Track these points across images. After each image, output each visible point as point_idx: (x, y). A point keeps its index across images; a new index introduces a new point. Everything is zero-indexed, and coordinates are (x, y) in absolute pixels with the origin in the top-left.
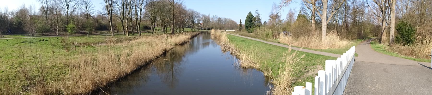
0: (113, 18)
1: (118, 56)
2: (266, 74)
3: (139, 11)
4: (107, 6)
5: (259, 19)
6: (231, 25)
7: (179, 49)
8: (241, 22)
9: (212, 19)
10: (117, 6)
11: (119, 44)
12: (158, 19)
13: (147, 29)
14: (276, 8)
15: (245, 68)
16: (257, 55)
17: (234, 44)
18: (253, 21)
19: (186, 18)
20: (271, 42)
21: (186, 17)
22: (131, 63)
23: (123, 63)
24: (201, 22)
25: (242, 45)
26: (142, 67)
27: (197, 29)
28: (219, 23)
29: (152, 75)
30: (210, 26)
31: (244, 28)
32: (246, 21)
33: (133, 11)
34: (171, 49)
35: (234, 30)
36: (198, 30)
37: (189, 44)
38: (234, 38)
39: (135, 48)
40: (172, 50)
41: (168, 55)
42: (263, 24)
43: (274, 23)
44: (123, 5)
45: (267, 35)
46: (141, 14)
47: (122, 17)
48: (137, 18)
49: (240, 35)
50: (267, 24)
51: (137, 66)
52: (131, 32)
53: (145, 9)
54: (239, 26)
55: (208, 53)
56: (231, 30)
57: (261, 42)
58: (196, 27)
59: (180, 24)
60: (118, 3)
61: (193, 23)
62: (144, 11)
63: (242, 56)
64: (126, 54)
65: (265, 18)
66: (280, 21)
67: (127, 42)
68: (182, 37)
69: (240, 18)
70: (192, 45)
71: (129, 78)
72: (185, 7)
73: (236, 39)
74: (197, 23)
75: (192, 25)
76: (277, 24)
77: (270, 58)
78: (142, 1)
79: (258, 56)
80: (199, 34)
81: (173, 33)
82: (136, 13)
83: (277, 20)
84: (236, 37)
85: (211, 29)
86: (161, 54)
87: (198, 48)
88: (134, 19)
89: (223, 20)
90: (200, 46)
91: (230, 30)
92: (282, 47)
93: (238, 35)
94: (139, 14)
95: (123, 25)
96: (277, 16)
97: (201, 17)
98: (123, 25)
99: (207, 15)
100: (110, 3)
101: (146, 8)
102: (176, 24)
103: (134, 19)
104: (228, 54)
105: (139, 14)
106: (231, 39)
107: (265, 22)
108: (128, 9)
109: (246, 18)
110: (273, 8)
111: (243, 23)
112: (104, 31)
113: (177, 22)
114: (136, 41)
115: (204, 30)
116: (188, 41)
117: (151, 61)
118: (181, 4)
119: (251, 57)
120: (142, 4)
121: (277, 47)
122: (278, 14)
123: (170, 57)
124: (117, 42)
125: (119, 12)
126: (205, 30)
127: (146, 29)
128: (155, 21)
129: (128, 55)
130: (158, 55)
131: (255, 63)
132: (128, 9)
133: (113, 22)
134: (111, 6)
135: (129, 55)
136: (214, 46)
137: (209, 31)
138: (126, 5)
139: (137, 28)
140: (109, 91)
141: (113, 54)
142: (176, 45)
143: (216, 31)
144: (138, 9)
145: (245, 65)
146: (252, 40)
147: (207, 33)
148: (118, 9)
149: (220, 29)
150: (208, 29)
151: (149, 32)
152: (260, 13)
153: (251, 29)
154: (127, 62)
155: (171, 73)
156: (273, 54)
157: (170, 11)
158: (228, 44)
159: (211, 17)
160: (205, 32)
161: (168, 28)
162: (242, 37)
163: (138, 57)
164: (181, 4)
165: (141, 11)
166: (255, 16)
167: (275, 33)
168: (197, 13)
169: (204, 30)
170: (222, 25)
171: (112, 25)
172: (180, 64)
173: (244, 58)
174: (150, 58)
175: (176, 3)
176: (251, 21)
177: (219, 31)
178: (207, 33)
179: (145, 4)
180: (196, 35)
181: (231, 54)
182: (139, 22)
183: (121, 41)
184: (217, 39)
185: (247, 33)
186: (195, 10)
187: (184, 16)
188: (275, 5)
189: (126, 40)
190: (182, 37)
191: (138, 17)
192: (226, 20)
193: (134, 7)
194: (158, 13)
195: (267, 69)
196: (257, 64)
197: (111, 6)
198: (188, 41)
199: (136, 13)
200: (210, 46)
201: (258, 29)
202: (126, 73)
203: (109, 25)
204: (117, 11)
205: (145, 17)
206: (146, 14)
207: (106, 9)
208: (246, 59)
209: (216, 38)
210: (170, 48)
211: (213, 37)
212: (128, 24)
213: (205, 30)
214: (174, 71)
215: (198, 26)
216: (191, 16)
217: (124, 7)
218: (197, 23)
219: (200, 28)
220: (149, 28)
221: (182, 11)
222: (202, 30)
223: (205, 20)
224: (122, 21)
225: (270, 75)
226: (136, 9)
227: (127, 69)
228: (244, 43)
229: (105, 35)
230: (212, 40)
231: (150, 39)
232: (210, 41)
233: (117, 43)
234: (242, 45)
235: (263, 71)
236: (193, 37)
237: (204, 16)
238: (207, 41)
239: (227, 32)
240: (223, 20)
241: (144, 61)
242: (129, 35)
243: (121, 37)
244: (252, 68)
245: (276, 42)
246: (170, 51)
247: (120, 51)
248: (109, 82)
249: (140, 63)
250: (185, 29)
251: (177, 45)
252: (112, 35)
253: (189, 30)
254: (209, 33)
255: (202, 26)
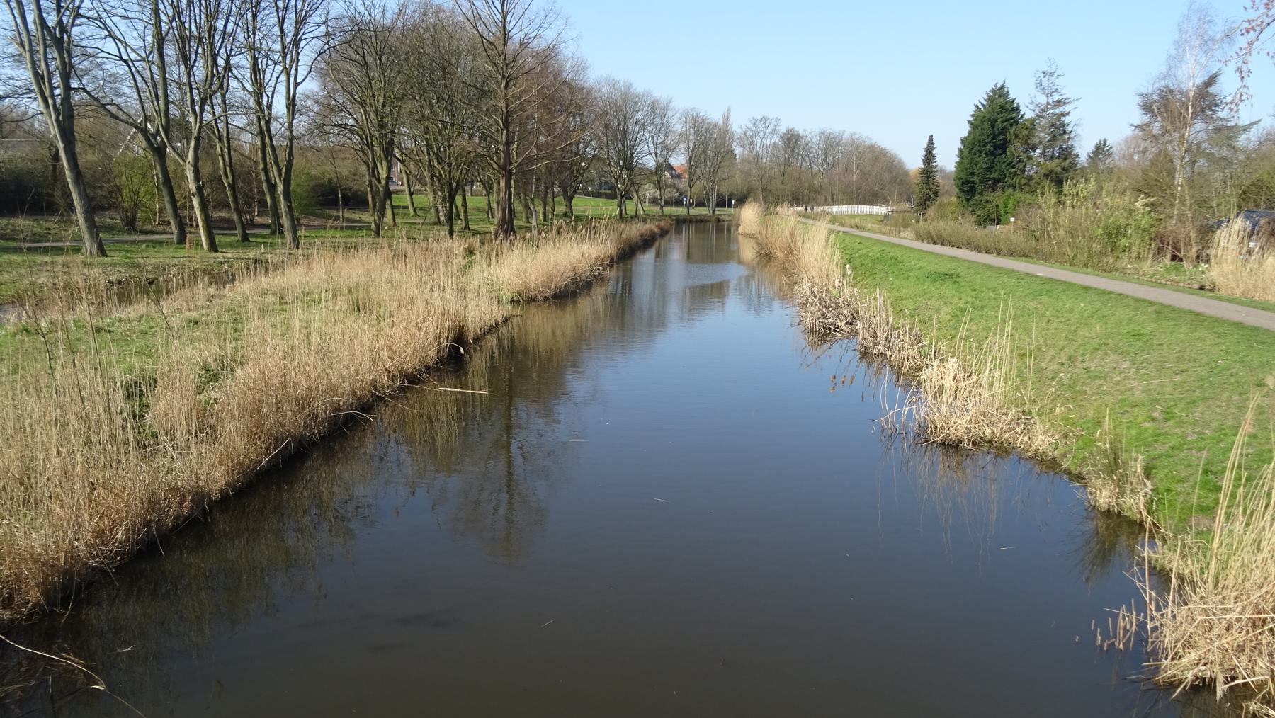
0: (82, 125)
1: (134, 391)
2: (1104, 496)
3: (282, 88)
4: (24, 41)
5: (1059, 130)
6: (861, 176)
7: (543, 327)
8: (929, 157)
9: (748, 140)
10: (110, 46)
11: (141, 308)
12: (407, 139)
13: (337, 204)
14: (1207, 43)
15: (951, 446)
16: (1039, 371)
17: (880, 297)
18: (1017, 148)
19: (587, 135)
20: (1144, 281)
21: (583, 126)
22: (235, 433)
23: (171, 433)
24: (679, 160)
25: (933, 304)
26: (307, 451)
27: (654, 201)
28: (787, 163)
29: (386, 490)
30: (737, 182)
31: (950, 196)
32: (970, 148)
33: (240, 88)
34: (493, 328)
35: (881, 210)
36: (655, 209)
37: (608, 296)
38: (880, 259)
39: (255, 326)
40: (503, 330)
41: (478, 363)
42: (1083, 159)
43: (1177, 152)
44: (160, 41)
45: (1113, 235)
46: (291, 105)
47: (159, 121)
48: (264, 133)
49: (919, 237)
50: (1117, 160)
51: (278, 440)
52: (229, 224)
53: (323, 74)
54: (916, 180)
55: (720, 348)
56: (865, 209)
57: (1071, 286)
58: (649, 191)
59: (549, 171)
60: (122, 27)
61: (629, 166)
62: (310, 87)
63: (930, 375)
64: (194, 373)
65: (1104, 120)
66: (1227, 134)
67: (202, 289)
68: (567, 255)
69: (927, 125)
70: (622, 302)
71: (222, 522)
72: (581, 67)
73: (897, 261)
74: (650, 163)
75: (622, 181)
76: (1194, 152)
77: (1139, 396)
78: (300, 23)
79: (1041, 378)
80: (664, 233)
81: (508, 228)
82: (259, 94)
83: (1197, 130)
84: (896, 253)
85: (742, 201)
86: (433, 353)
87: (657, 322)
88: (248, 141)
89: (816, 144)
90: (673, 309)
91: (855, 209)
92: (1240, 326)
93: (907, 239)
94: (280, 106)
95: (167, 180)
96: (1205, 99)
97: (679, 127)
98: (167, 180)
99: (714, 115)
100: (51, 20)
101: (328, 67)
102: (524, 173)
103: (248, 141)
104: (840, 354)
105: (280, 106)
106: (865, 265)
107: (1100, 150)
108: (200, 73)
109: (965, 130)
110: (1180, 45)
111: (948, 160)
112: (20, 222)
113: (530, 160)
114: (264, 282)
115: (698, 205)
116: (601, 279)
117: (369, 403)
118: (552, 50)
119: (993, 381)
120: (296, 42)
121: (1196, 318)
122: (1211, 81)
123: (490, 375)
124: (123, 292)
125: (127, 88)
126: (703, 211)
127: (333, 204)
128: (388, 154)
129: (211, 375)
130: (412, 365)
131: (1025, 418)
132: (200, 73)
133: (87, 158)
134: (59, 39)
135: (215, 378)
136: (755, 305)
137: (724, 212)
138: (183, 39)
139: (265, 201)
140: (76, 636)
141: (92, 380)
142: (524, 300)
143: (766, 214)
144: (272, 73)
145: (959, 427)
146: (1002, 272)
147: (711, 227)
148: (122, 69)
149: (796, 200)
150: (721, 204)
151: (351, 226)
152: (1067, 93)
153: (997, 198)
154: (205, 423)
155: (499, 468)
156: (1162, 368)
157: (484, 94)
158: (846, 292)
159: (738, 125)
160: (700, 221)
161: (476, 201)
162: (938, 249)
163: (283, 386)
164: (552, 50)
165: (292, 91)
166: (1029, 115)
167: (1180, 224)
168: (654, 106)
169: (695, 211)
170: (801, 176)
171: (78, 175)
172: (548, 414)
173: (948, 383)
174: (363, 385)
175: (523, 44)
176: (1003, 147)
177: (788, 216)
178: (711, 227)
179: (317, 44)
180: (647, 242)
181: (865, 354)
182: (283, 157)
183: (154, 288)
184: (774, 268)
185: (967, 226)
186: (640, 86)
187: (573, 122)
188: (1205, 18)
189: (190, 280)
190: (567, 255)
191: (274, 127)
192: (832, 143)
193: (242, 61)
194: (408, 106)
195: (1114, 466)
196: (1039, 428)
197: (59, 43)
198: (601, 279)
199: (259, 94)
200: (734, 305)
201: (1048, 198)
202: (200, 498)
203: (57, 175)
204: (115, 78)
205: (320, 129)
206: (328, 107)
207: (18, 59)
208: (964, 391)
209: (766, 256)
210: (488, 320)
211: (748, 252)
212: (206, 169)
213: (703, 211)
214: (518, 461)
215: (659, 185)
216: (618, 121)
217: (171, 51)
218: (650, 163)
219: (670, 193)
220: (356, 201)
221: (560, 95)
222: (681, 211)
223: (705, 144)
224: (159, 152)
225: (1135, 504)
226: (255, 70)
227: (206, 467)
228: (947, 289)
229: (37, 245)
230: (743, 271)
231: (363, 267)
232: (733, 272)
233: (124, 298)
234: (933, 304)
235: (1080, 477)
236: (627, 254)
237: (697, 123)
238: (710, 274)
239: (834, 219)
240: (816, 144)
241: (320, 406)
242: (214, 247)
243: (153, 259)
244: (1002, 450)
245: (1175, 286)
246: (491, 341)
247: (147, 352)
248: (67, 572)
249: (294, 422)
250: (583, 204)
251: (531, 300)
252: (88, 244)
253: (608, 208)
254: (724, 229)
255: (683, 184)
